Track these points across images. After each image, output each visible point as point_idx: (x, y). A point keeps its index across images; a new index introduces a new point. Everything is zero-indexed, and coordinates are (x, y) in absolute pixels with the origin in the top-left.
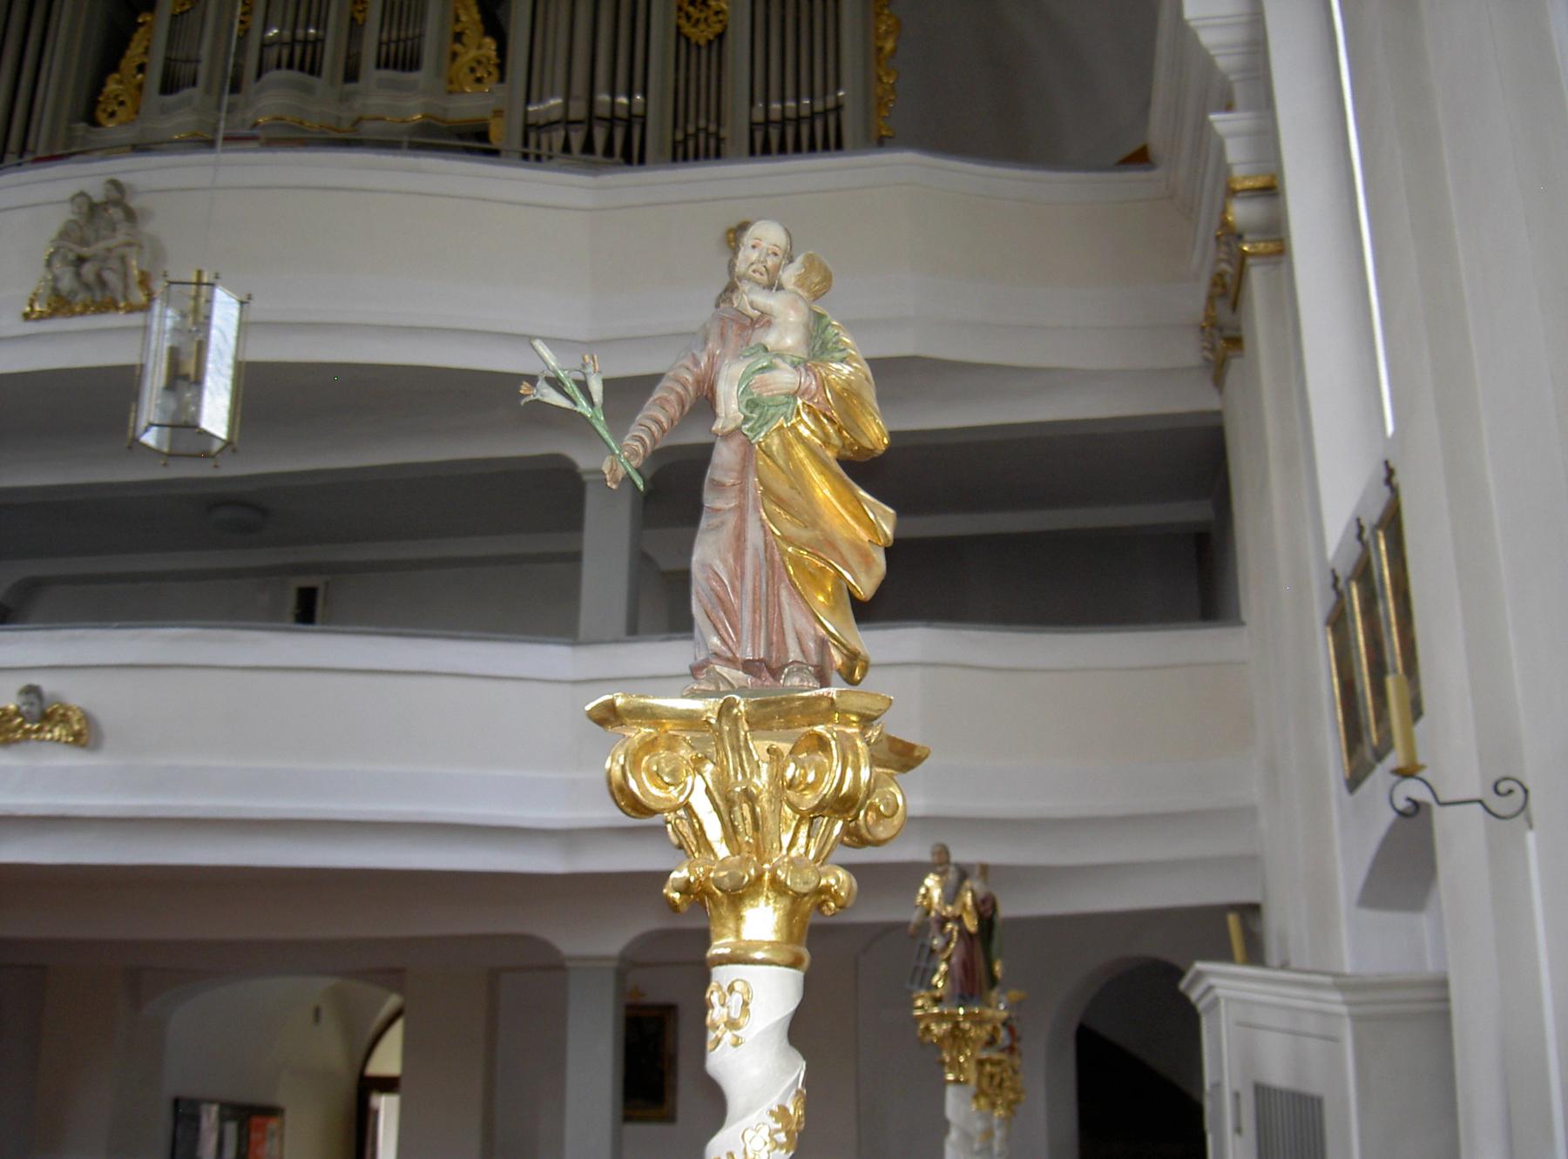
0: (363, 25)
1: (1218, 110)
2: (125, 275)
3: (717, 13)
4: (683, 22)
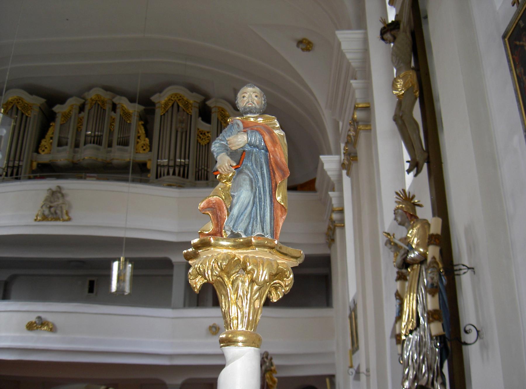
0: (113, 132)
1: (331, 191)
2: (62, 212)
3: (208, 137)
4: (199, 139)
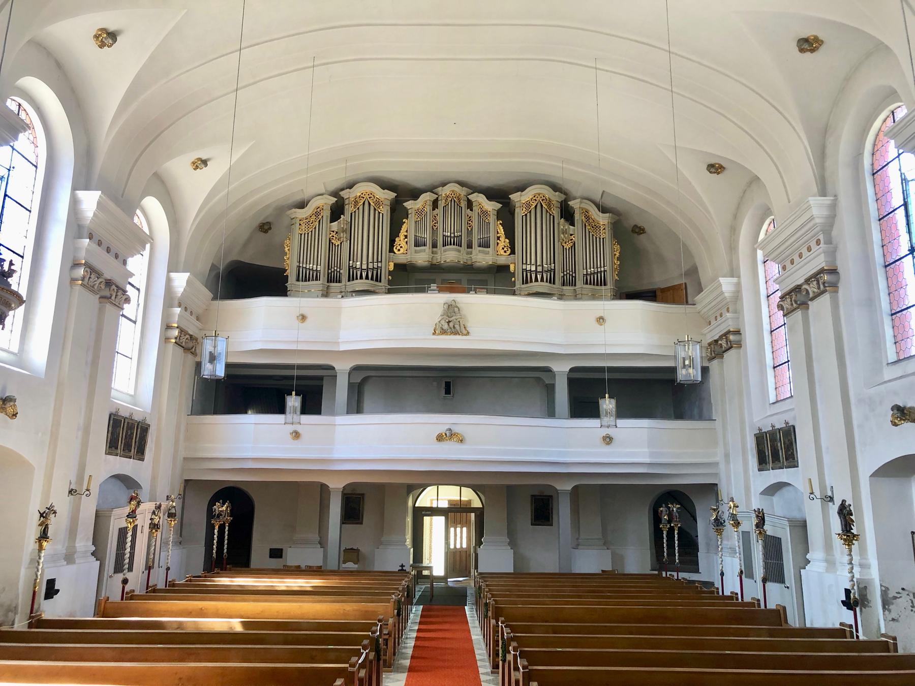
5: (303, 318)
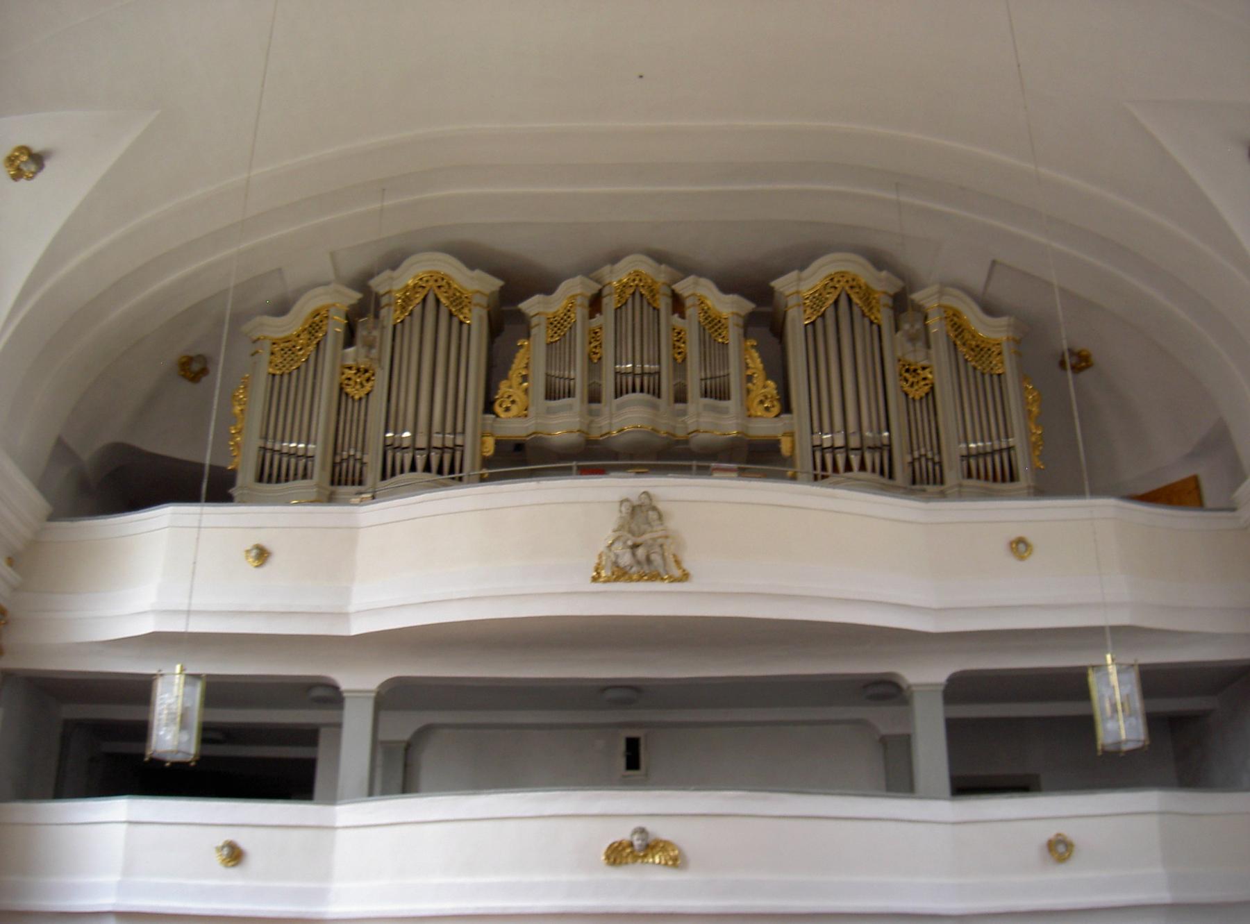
3: (925, 379)
5: (262, 555)
